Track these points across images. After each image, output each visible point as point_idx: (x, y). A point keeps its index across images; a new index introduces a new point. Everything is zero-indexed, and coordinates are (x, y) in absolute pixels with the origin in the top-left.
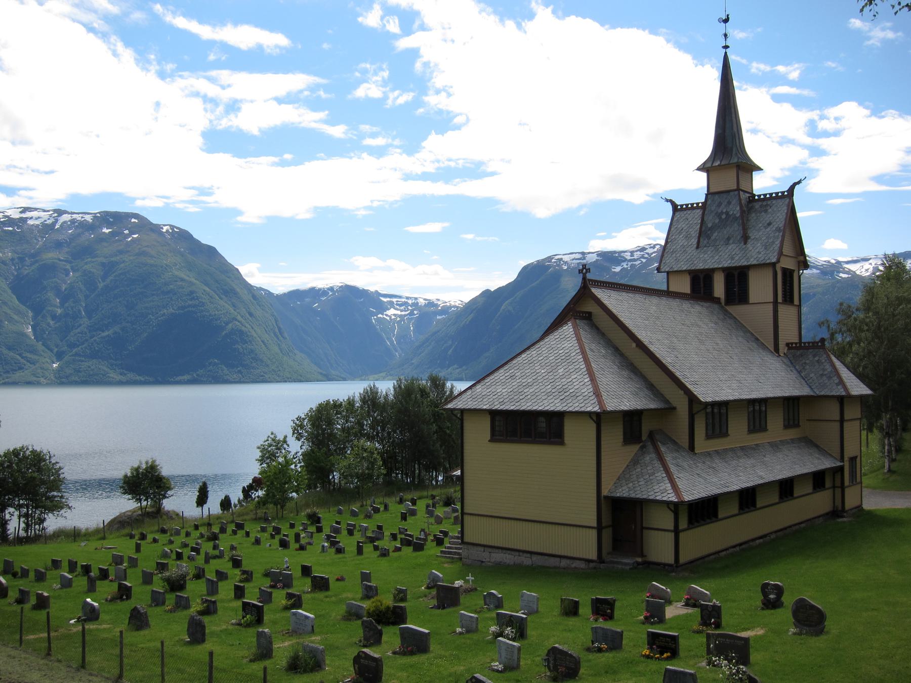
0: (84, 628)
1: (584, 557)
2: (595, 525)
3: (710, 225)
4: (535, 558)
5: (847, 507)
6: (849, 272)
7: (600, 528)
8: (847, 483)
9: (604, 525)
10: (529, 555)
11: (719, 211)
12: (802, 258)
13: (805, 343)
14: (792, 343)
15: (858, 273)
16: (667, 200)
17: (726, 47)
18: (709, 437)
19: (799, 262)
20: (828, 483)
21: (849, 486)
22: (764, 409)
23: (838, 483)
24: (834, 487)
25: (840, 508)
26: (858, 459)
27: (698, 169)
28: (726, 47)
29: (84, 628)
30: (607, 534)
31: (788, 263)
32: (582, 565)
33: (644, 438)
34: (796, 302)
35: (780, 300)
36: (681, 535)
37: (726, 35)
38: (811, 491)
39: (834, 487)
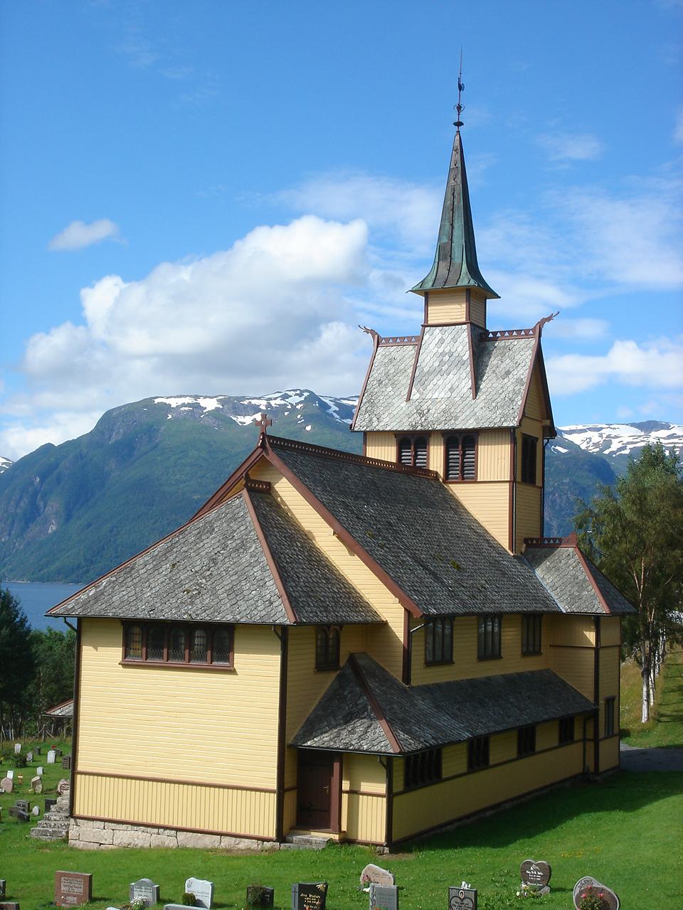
0: (347, 792)
1: (256, 834)
2: (274, 786)
3: (426, 370)
4: (181, 835)
5: (602, 768)
6: (570, 445)
7: (281, 791)
8: (602, 734)
9: (286, 786)
10: (173, 832)
11: (440, 351)
12: (547, 422)
13: (549, 540)
14: (532, 539)
15: (583, 447)
16: (367, 331)
17: (459, 124)
18: (428, 664)
19: (544, 428)
20: (578, 735)
21: (605, 739)
22: (496, 629)
23: (590, 735)
24: (584, 740)
25: (592, 769)
26: (617, 699)
27: (500, 297)
28: (459, 124)
29: (347, 792)
30: (290, 798)
31: (534, 430)
32: (254, 845)
33: (342, 664)
34: (539, 483)
35: (519, 478)
36: (396, 800)
37: (459, 108)
38: (556, 743)
39: (584, 740)
